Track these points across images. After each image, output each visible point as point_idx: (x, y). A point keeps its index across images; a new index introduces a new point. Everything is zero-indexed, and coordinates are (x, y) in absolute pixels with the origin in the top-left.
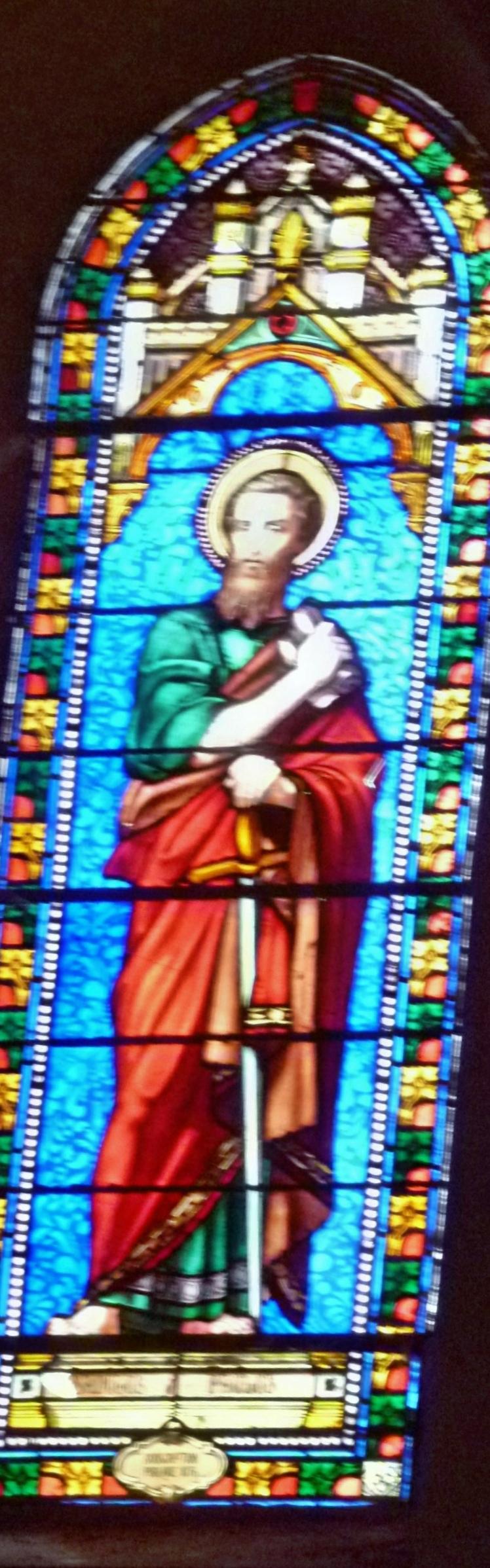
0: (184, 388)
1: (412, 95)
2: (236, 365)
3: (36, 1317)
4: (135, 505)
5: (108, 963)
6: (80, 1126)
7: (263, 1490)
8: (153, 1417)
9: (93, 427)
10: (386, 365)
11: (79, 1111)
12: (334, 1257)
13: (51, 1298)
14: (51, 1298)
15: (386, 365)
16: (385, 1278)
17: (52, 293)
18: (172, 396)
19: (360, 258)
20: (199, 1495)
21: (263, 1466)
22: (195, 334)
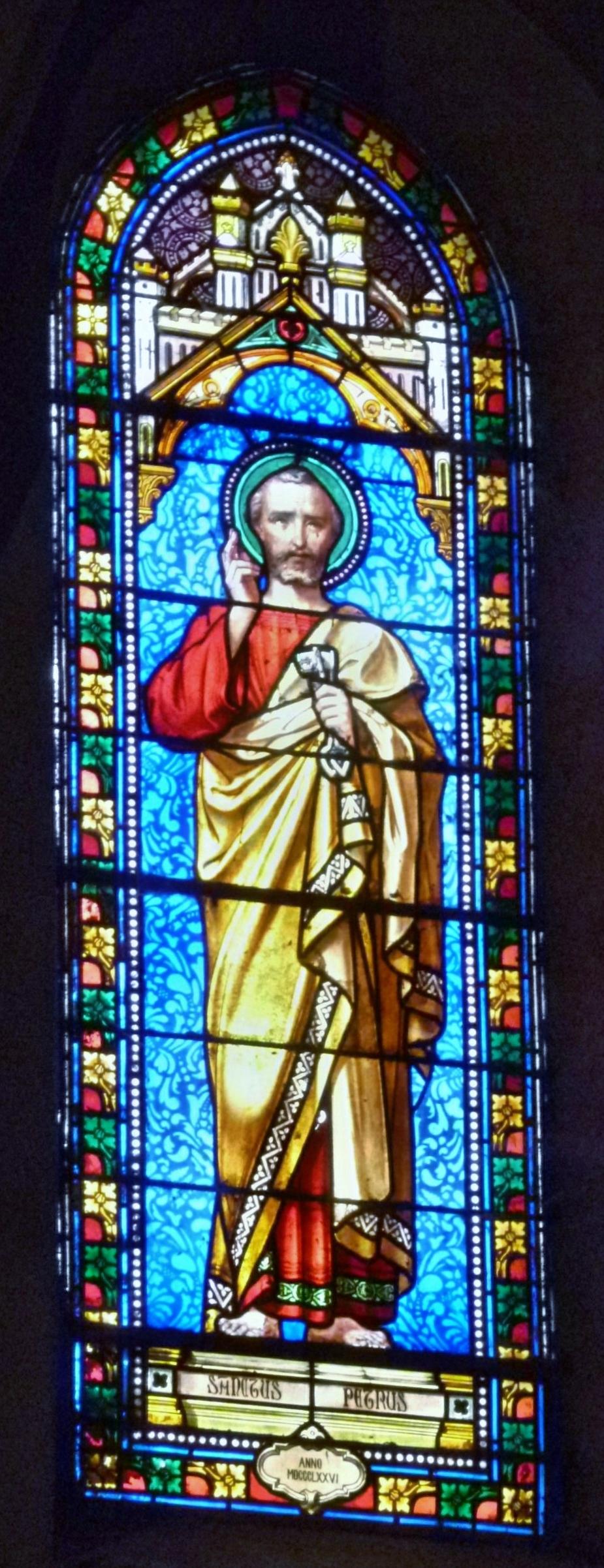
0: (200, 374)
1: (384, 296)
2: (250, 362)
3: (159, 1310)
4: (164, 488)
5: (194, 1236)
6: (177, 1119)
7: (403, 1506)
8: (286, 1425)
9: (113, 407)
10: (399, 388)
11: (174, 826)
12: (445, 1280)
13: (171, 1293)
14: (171, 1293)
15: (399, 388)
16: (497, 1319)
17: (110, 1318)
18: (193, 377)
19: (361, 278)
20: (338, 1504)
21: (402, 1483)
22: (208, 324)
